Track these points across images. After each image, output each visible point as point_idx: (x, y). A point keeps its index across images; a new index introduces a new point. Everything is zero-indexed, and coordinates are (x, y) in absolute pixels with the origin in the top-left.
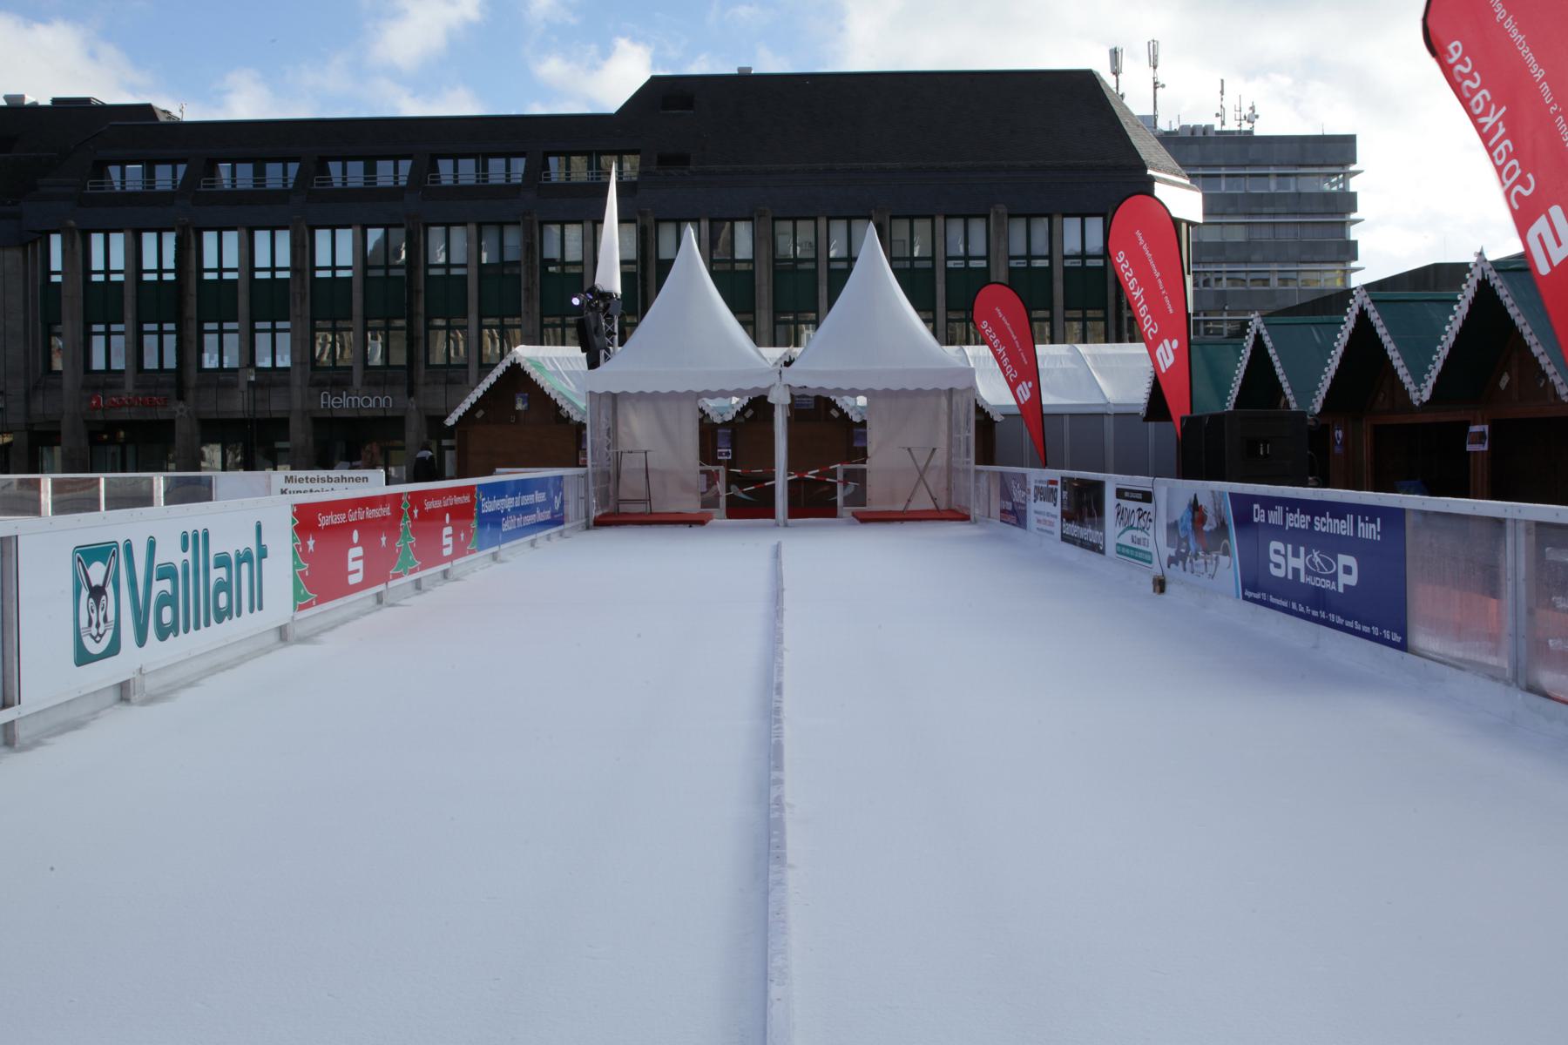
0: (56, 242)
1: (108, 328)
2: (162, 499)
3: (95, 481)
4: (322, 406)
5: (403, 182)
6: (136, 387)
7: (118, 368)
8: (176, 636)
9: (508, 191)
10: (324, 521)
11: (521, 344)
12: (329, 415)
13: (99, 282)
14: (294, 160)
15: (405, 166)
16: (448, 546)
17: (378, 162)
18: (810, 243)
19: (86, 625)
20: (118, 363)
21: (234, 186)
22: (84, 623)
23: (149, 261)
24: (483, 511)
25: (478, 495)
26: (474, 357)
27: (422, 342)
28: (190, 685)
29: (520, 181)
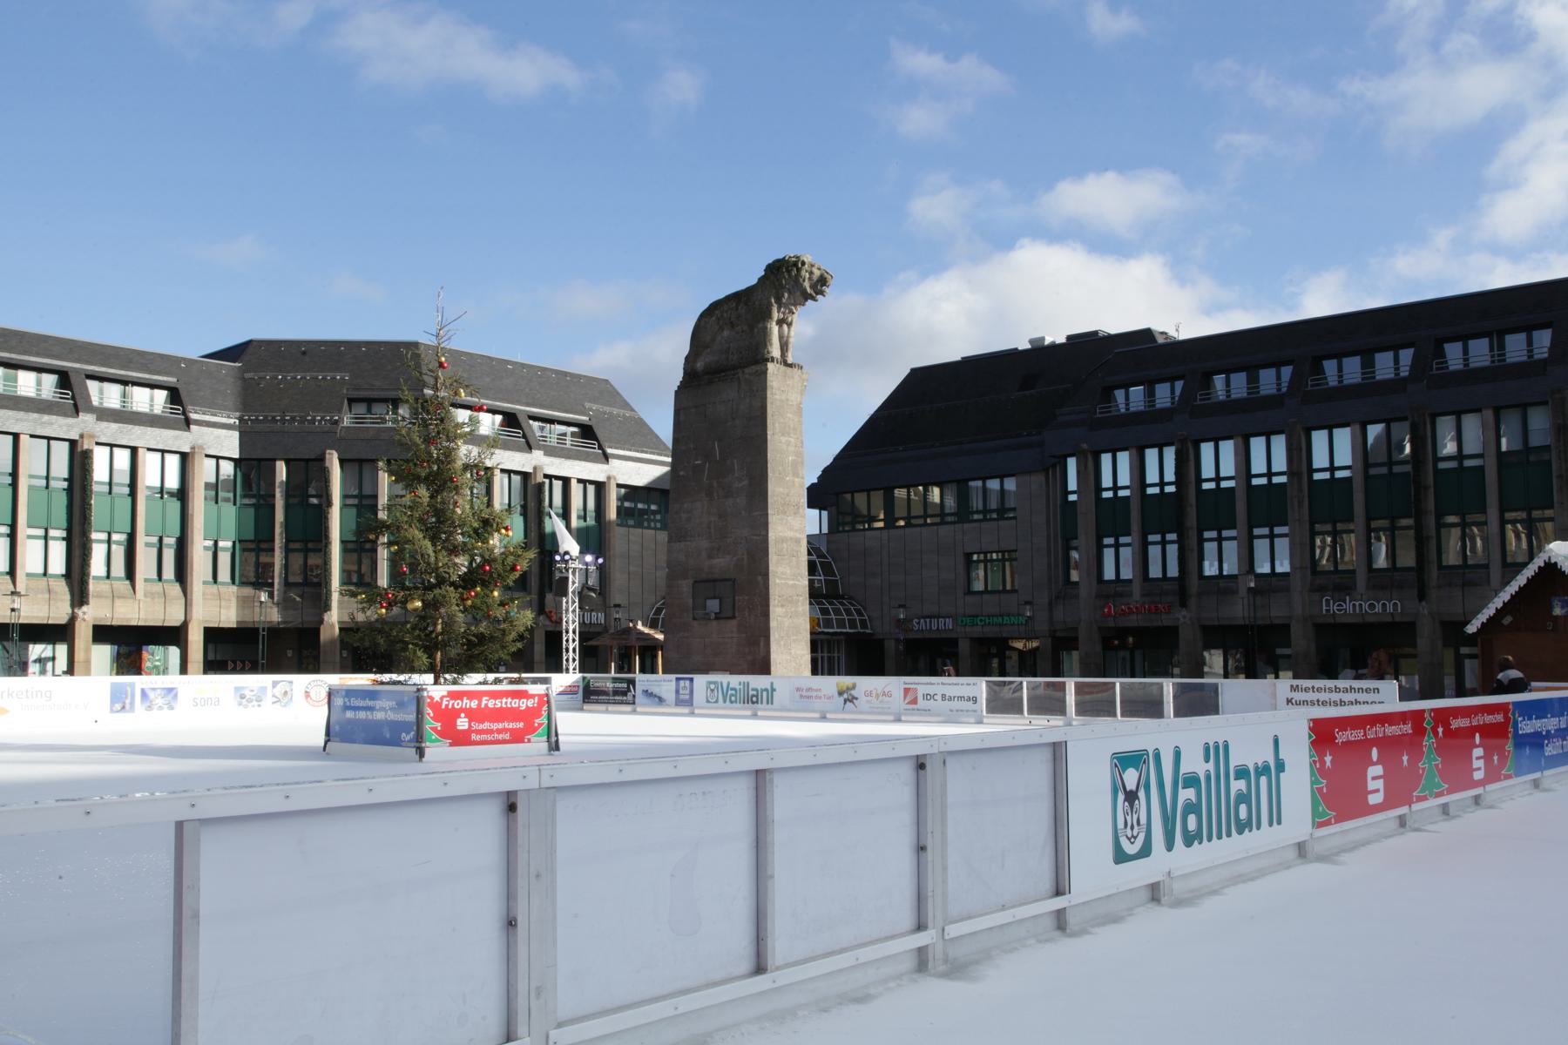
0: (1072, 464)
1: (1117, 540)
2: (1172, 705)
3: (1111, 685)
4: (1324, 612)
5: (1404, 372)
6: (1143, 595)
7: (1126, 578)
8: (1200, 843)
9: (1530, 368)
10: (1342, 737)
11: (1555, 540)
12: (1331, 621)
13: (1263, 485)
14: (1180, 378)
15: (1406, 355)
16: (1479, 769)
17: (1261, 371)
19: (1123, 827)
20: (1127, 573)
21: (1229, 396)
22: (1120, 825)
23: (1152, 476)
24: (1520, 732)
25: (1514, 714)
26: (1496, 556)
27: (1433, 542)
28: (1215, 892)
29: (1546, 355)
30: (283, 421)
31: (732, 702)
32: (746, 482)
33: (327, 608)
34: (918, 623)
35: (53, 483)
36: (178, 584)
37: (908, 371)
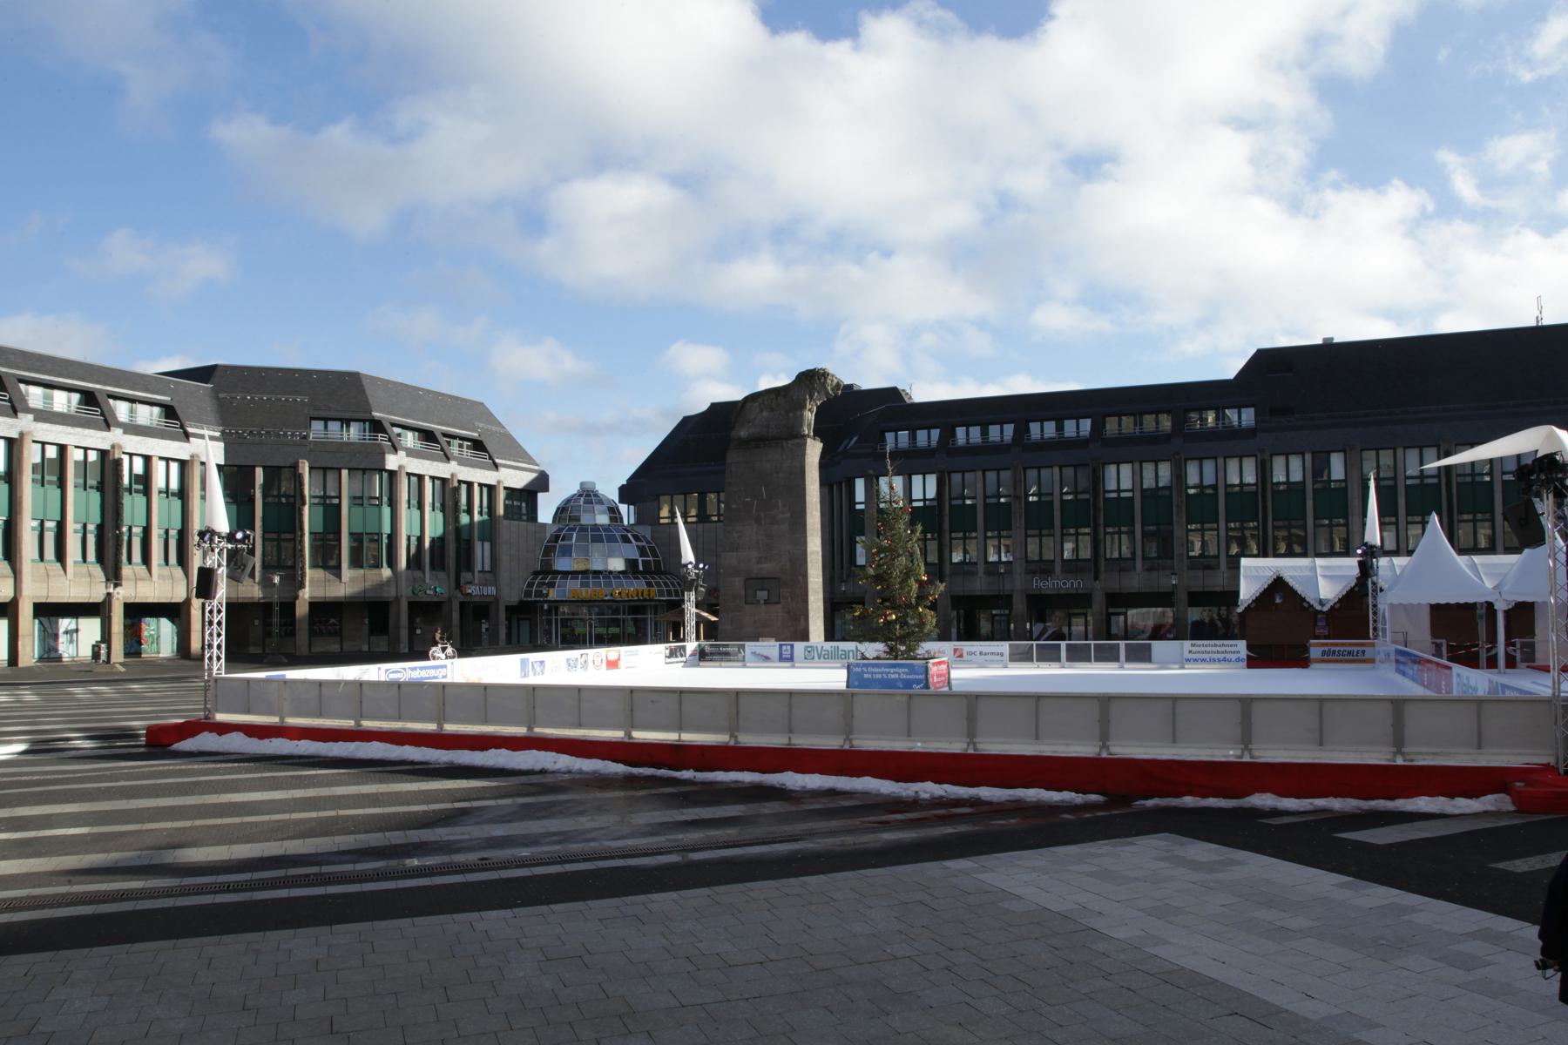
18: (1388, 466)
27: (1102, 543)
30: (259, 433)
31: (825, 658)
32: (788, 515)
33: (302, 586)
36: (180, 568)
37: (709, 405)
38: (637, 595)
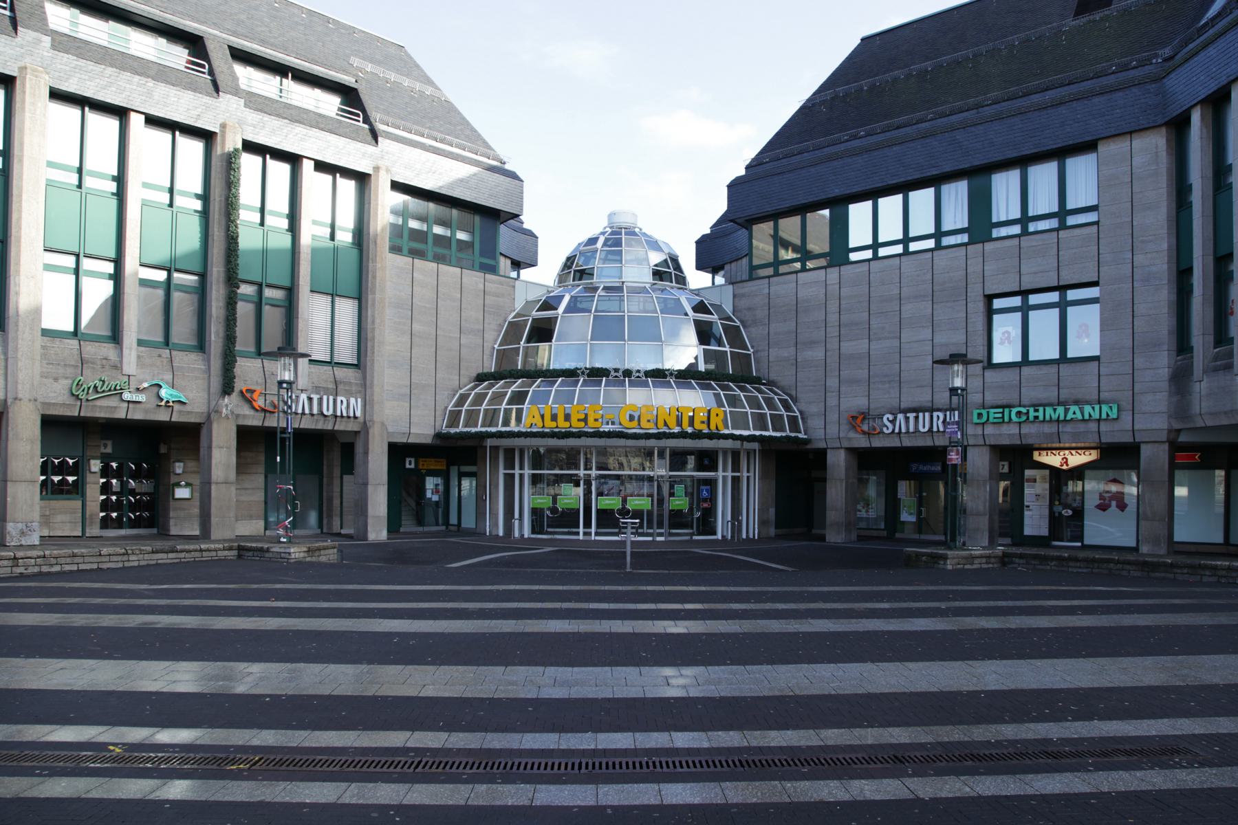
34: (893, 422)
35: (179, 201)
38: (679, 423)
